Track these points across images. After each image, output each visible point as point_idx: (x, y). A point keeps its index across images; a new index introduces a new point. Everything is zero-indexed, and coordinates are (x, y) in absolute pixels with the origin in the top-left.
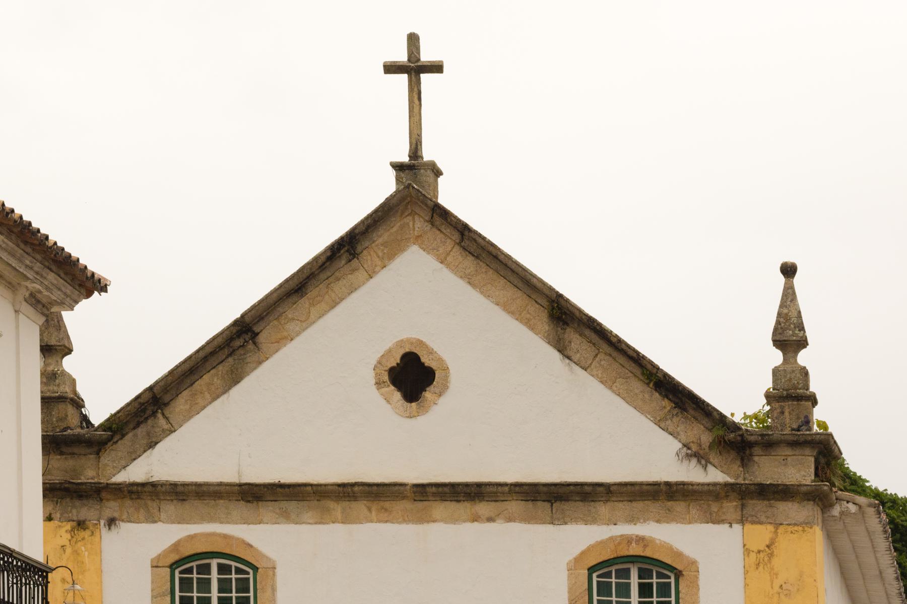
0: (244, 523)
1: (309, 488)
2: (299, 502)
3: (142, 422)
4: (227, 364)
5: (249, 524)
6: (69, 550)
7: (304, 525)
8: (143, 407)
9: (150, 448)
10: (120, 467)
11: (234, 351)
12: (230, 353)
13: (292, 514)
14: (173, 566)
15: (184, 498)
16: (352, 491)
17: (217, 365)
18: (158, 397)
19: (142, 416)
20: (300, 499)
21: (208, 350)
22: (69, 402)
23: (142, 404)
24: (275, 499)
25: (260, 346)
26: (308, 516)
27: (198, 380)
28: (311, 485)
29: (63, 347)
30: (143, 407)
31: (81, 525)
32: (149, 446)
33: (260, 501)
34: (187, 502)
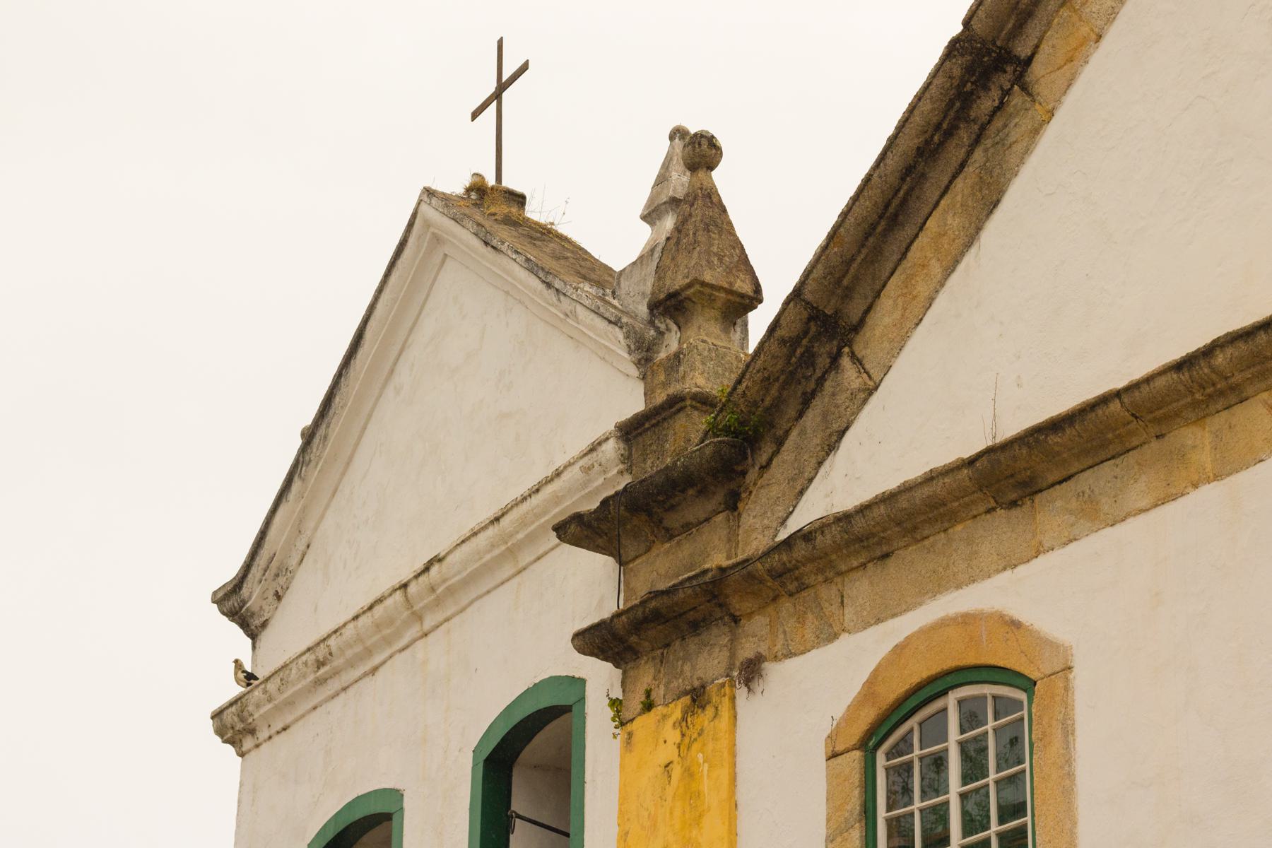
0: (1005, 569)
1: (1115, 406)
2: (1118, 461)
3: (813, 394)
4: (971, 169)
5: (1015, 566)
6: (677, 771)
7: (1130, 520)
8: (799, 351)
9: (831, 451)
10: (775, 525)
11: (983, 128)
12: (974, 136)
13: (1103, 501)
14: (869, 743)
15: (885, 549)
16: (1213, 370)
17: (951, 182)
18: (828, 311)
19: (811, 376)
20: (1119, 449)
21: (910, 143)
22: (692, 406)
23: (793, 342)
24: (1065, 474)
25: (1036, 89)
26: (1137, 493)
27: (916, 236)
28: (1117, 394)
29: (697, 287)
30: (799, 351)
31: (698, 697)
32: (826, 448)
33: (1036, 492)
34: (893, 558)
